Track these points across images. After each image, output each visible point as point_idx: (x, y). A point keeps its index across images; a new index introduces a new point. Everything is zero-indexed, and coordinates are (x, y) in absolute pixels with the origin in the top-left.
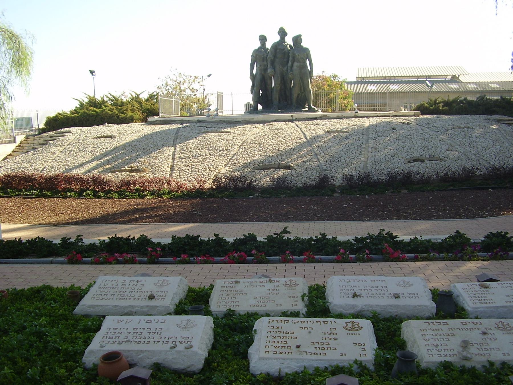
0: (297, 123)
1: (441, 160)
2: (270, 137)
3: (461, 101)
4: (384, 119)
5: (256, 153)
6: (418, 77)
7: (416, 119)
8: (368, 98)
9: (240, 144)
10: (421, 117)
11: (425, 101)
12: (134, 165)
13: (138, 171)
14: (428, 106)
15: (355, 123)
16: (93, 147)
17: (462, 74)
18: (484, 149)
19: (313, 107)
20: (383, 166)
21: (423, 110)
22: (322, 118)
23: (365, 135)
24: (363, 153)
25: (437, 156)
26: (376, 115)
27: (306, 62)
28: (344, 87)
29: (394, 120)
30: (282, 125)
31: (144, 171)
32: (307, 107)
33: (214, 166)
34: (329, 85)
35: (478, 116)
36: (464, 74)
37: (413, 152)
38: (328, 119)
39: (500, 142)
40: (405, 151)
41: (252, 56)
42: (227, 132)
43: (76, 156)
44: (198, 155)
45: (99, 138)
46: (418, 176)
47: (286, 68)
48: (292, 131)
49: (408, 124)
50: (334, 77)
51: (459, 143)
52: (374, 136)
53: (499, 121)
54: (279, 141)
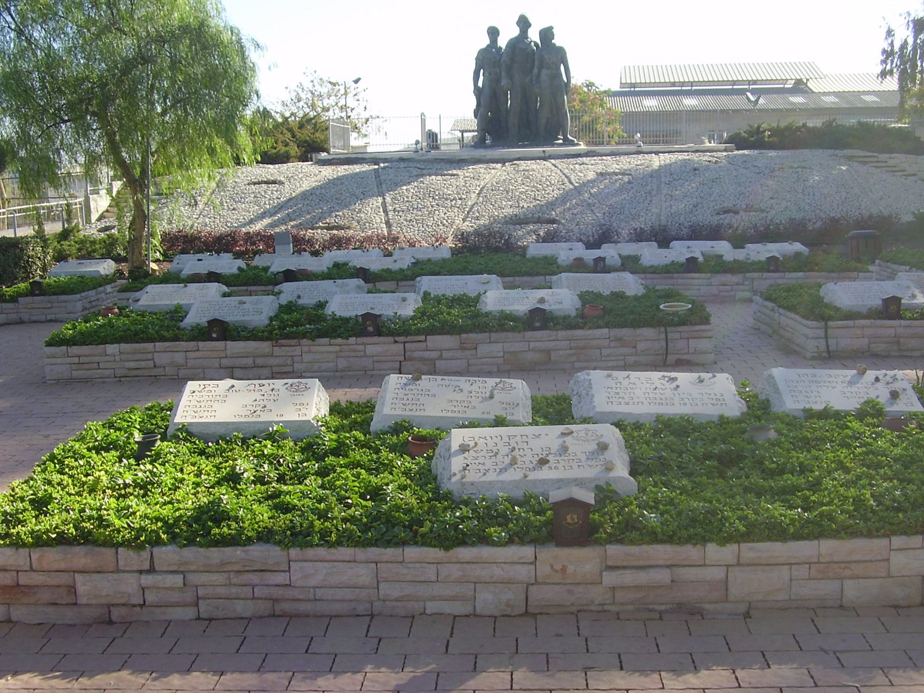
0: (553, 161)
1: (762, 211)
2: (519, 182)
3: (798, 129)
4: (681, 156)
5: (504, 203)
6: (734, 83)
7: (728, 156)
8: (643, 122)
9: (477, 192)
10: (736, 152)
11: (741, 127)
12: (331, 220)
13: (339, 228)
14: (746, 136)
15: (639, 162)
16: (255, 197)
17: (812, 77)
18: (823, 196)
19: (571, 138)
20: (682, 219)
21: (738, 142)
22: (587, 154)
23: (655, 179)
24: (654, 202)
25: (757, 206)
26: (669, 150)
27: (559, 68)
28: (606, 103)
29: (695, 157)
30: (532, 165)
31: (349, 228)
32: (560, 139)
33: (449, 221)
34: (581, 101)
35: (821, 151)
36: (817, 76)
37: (724, 201)
38: (598, 156)
39: (847, 187)
40: (712, 199)
41: (477, 59)
42: (454, 175)
43: (234, 209)
44: (420, 206)
45: (255, 184)
46: (730, 231)
47: (527, 79)
48: (549, 174)
49: (716, 162)
50: (587, 86)
51: (789, 189)
52: (668, 179)
53: (850, 158)
54: (534, 187)
